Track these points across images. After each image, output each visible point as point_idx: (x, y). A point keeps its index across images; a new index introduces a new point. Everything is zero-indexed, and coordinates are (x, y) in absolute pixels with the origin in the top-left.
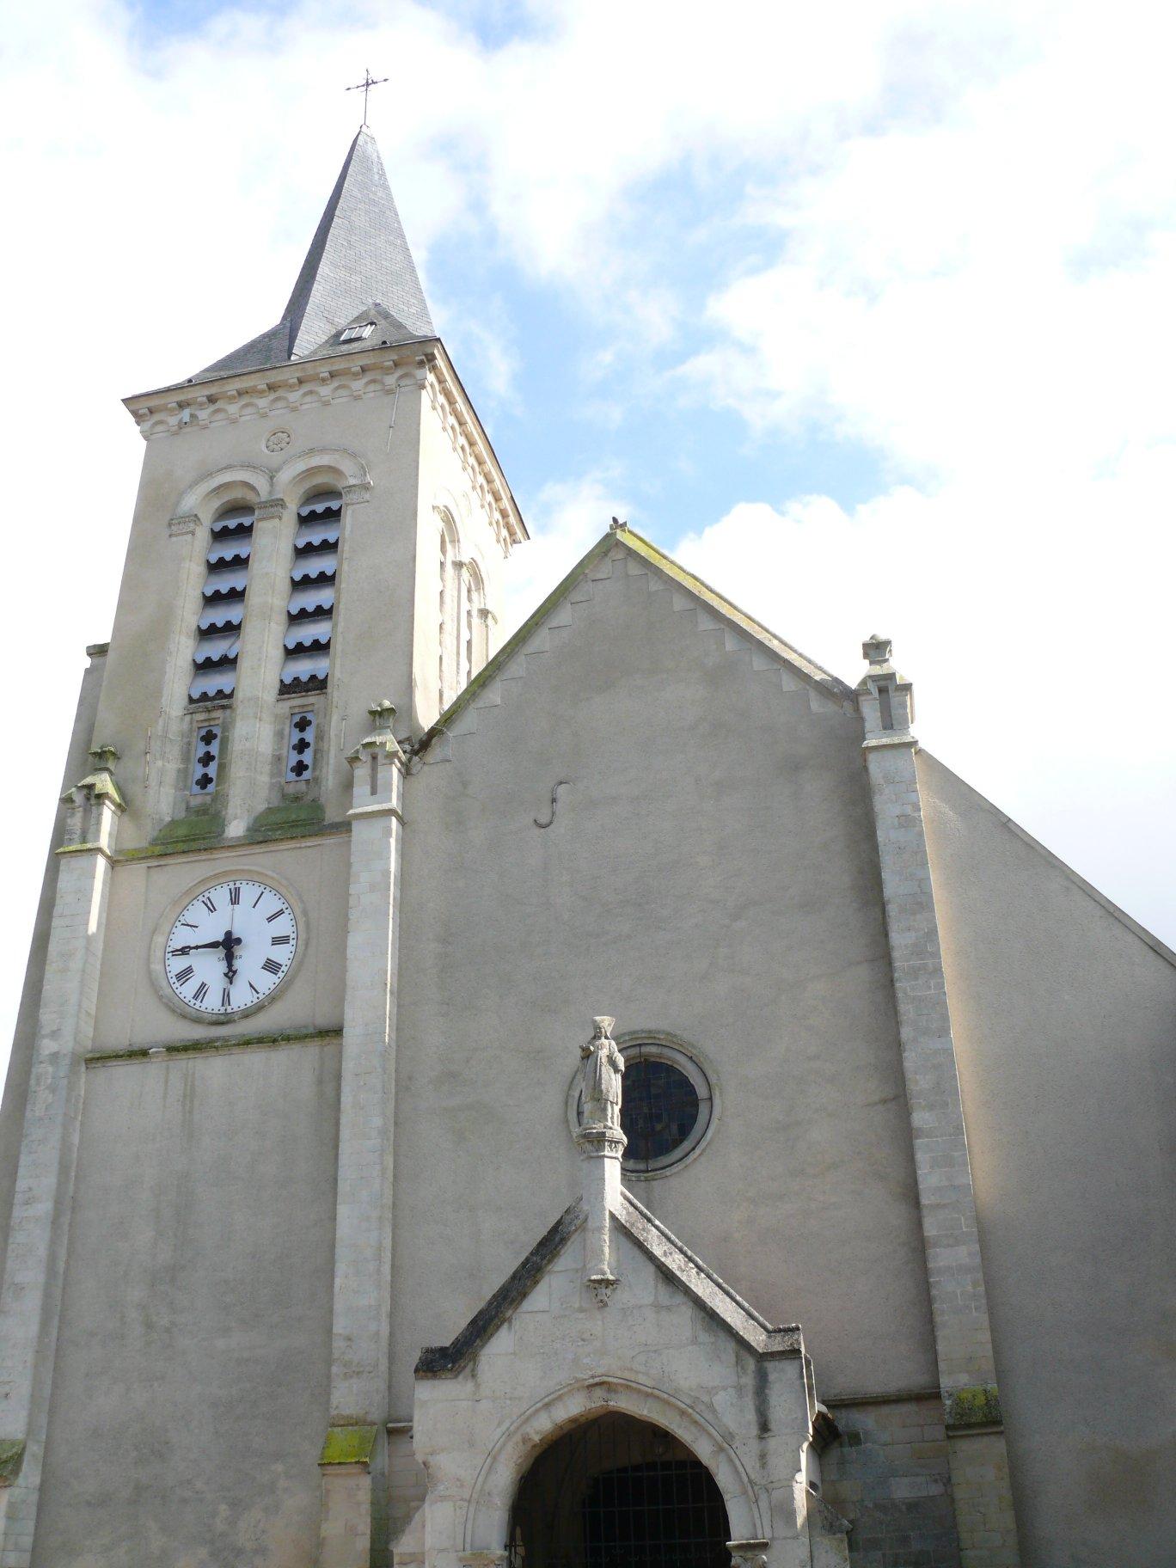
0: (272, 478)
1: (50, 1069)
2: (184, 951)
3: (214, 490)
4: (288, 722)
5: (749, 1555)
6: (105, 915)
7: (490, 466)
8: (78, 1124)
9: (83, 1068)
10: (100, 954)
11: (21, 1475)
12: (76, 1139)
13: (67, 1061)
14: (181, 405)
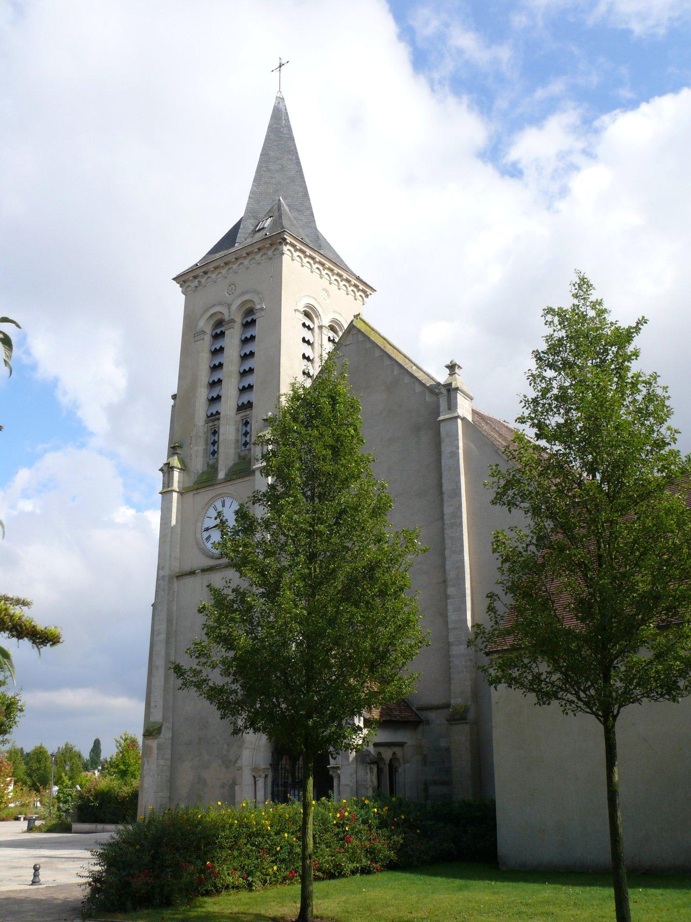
0: (229, 308)
1: (162, 582)
2: (207, 529)
3: (210, 316)
4: (241, 423)
5: (334, 770)
6: (180, 516)
7: (336, 270)
8: (175, 603)
9: (175, 580)
10: (179, 533)
11: (162, 734)
12: (175, 608)
13: (167, 579)
14: (195, 277)
